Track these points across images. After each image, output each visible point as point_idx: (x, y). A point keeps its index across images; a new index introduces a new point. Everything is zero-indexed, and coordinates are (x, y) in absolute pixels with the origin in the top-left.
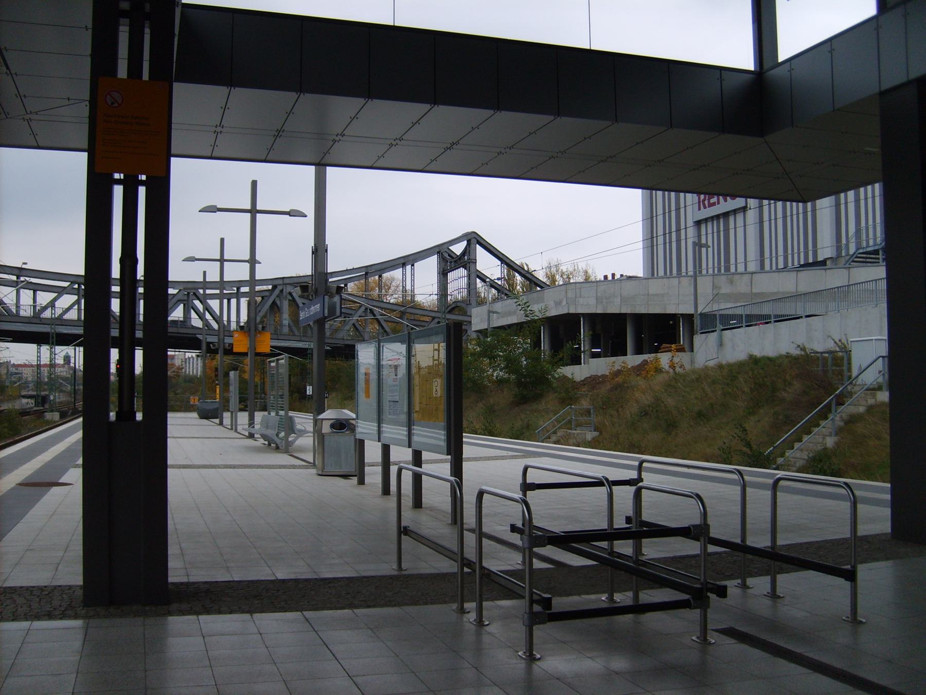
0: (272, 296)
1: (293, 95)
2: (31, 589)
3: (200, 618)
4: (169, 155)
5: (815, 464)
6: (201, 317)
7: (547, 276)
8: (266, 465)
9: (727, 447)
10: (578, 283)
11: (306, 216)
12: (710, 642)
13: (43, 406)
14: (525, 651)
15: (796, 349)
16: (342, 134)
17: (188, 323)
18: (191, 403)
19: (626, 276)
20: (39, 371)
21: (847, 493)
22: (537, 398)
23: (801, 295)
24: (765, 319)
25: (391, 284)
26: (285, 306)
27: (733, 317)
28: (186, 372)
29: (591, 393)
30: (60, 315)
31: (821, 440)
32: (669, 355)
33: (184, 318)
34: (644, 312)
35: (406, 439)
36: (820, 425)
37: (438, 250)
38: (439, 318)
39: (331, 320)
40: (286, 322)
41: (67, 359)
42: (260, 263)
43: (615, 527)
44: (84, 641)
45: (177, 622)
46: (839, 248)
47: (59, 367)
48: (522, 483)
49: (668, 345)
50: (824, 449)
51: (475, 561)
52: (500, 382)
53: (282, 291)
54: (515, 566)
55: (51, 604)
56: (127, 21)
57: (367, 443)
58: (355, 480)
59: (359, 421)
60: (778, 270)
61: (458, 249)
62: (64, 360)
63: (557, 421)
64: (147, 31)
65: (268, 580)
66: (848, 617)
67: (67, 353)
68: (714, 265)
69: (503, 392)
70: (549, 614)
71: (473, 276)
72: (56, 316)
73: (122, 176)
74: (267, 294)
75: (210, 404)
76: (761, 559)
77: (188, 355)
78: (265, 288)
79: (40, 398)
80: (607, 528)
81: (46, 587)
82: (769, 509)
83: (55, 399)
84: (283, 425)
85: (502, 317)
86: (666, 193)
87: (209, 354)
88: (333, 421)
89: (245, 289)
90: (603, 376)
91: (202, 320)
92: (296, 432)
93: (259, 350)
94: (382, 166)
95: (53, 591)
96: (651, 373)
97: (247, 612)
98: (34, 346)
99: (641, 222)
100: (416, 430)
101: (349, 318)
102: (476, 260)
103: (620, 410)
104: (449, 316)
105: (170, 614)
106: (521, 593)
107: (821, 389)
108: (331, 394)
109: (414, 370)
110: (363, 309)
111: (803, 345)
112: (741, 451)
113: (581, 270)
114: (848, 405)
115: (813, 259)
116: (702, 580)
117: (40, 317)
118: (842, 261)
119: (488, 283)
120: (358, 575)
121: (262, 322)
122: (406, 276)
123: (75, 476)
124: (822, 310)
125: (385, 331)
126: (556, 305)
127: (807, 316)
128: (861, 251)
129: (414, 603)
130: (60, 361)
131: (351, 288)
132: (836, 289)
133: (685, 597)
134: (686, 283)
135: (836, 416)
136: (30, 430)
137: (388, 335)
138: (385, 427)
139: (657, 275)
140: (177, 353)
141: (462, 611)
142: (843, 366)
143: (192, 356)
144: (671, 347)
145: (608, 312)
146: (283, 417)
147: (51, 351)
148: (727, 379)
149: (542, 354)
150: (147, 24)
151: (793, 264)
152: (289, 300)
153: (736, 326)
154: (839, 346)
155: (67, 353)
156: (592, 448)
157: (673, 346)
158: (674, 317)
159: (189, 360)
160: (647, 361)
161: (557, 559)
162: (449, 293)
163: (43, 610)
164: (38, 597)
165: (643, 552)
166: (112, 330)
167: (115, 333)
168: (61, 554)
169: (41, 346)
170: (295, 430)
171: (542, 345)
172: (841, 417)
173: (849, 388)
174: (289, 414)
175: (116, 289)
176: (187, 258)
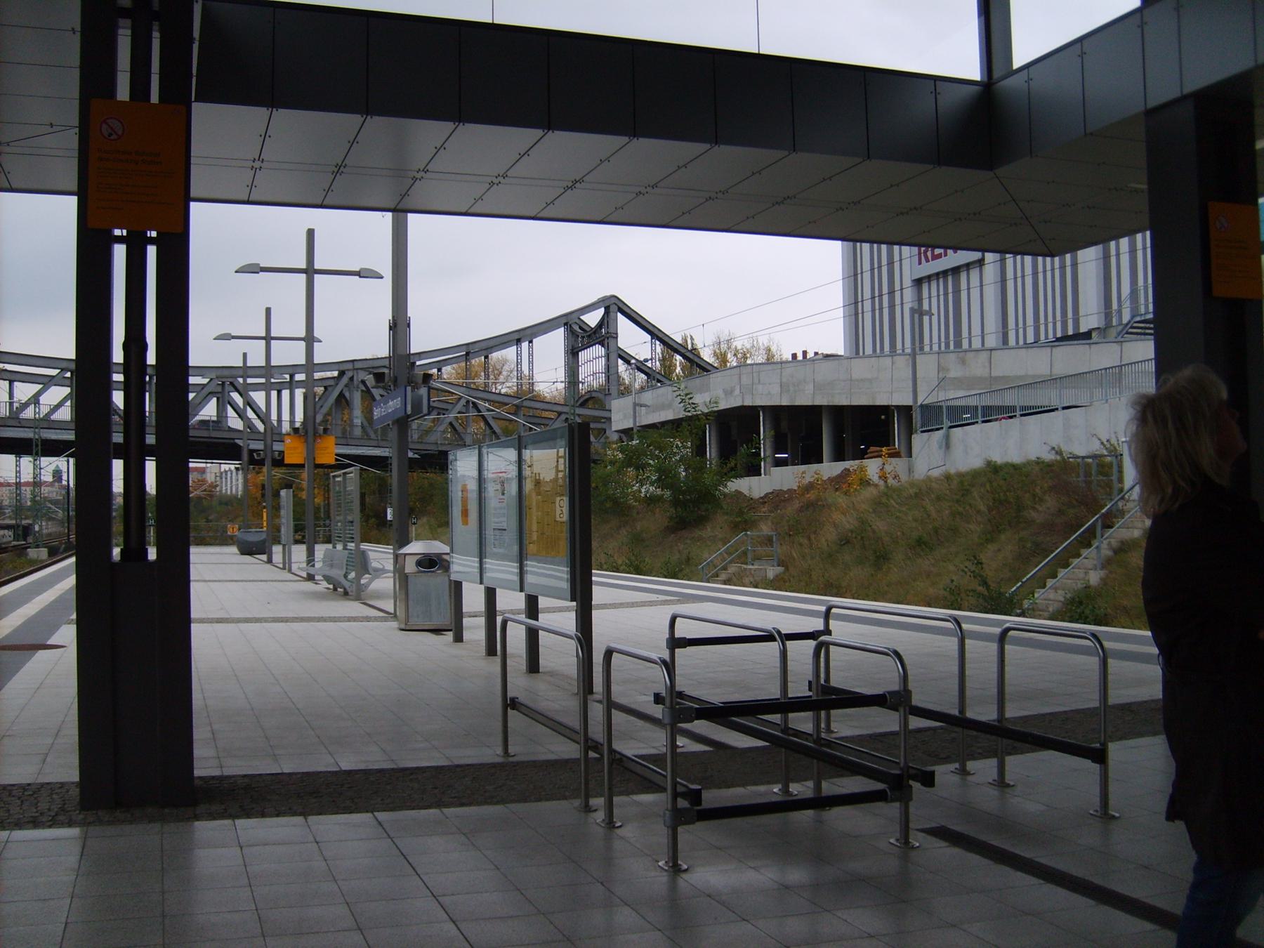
0: (339, 386)
1: (357, 119)
2: (9, 788)
3: (236, 824)
4: (187, 199)
5: (1074, 608)
6: (241, 414)
7: (715, 354)
8: (330, 617)
9: (956, 586)
10: (757, 364)
11: (382, 278)
12: (913, 846)
13: (25, 540)
14: (667, 860)
15: (1049, 453)
16: (425, 170)
17: (224, 423)
18: (229, 533)
19: (822, 354)
20: (18, 492)
21: (1092, 644)
22: (701, 521)
23: (1056, 379)
24: (1008, 412)
25: (502, 368)
26: (357, 399)
27: (966, 409)
28: (221, 491)
29: (772, 514)
30: (46, 414)
31: (1082, 575)
32: (878, 461)
33: (218, 416)
34: (845, 403)
35: (516, 578)
36: (1081, 556)
37: (565, 322)
38: (567, 413)
39: (419, 418)
40: (358, 421)
41: (57, 474)
42: (321, 341)
43: (790, 696)
44: (82, 855)
45: (206, 829)
46: (1108, 316)
47: (46, 486)
48: (669, 638)
49: (878, 449)
50: (1086, 587)
51: (602, 742)
52: (651, 500)
53: (352, 379)
54: (661, 748)
55: (36, 808)
56: (128, 22)
57: (465, 585)
58: (449, 636)
59: (454, 555)
60: (1027, 346)
61: (592, 319)
62: (54, 477)
63: (727, 553)
64: (156, 35)
65: (330, 772)
66: (1097, 811)
67: (57, 466)
68: (1017, 324)
69: (655, 514)
70: (699, 811)
71: (613, 356)
72: (41, 416)
73: (125, 233)
74: (332, 382)
75: (254, 537)
76: (988, 736)
77: (224, 467)
78: (329, 374)
79: (21, 528)
80: (779, 697)
81: (29, 785)
82: (957, 662)
83: (41, 529)
84: (353, 562)
85: (654, 412)
86: (875, 245)
87: (252, 466)
88: (420, 556)
89: (300, 377)
90: (790, 491)
91: (242, 420)
92: (371, 571)
93: (319, 461)
94: (479, 211)
95: (39, 790)
96: (855, 487)
97: (300, 814)
98: (12, 458)
99: (841, 281)
100: (530, 565)
101: (444, 414)
102: (617, 334)
103: (813, 536)
104: (579, 411)
105: (197, 818)
106: (662, 784)
107: (1082, 507)
108: (420, 519)
109: (528, 486)
110: (463, 402)
111: (1059, 447)
112: (974, 591)
113: (762, 347)
114: (1118, 528)
115: (1073, 330)
116: (902, 765)
117: (18, 418)
118: (1113, 333)
119: (633, 366)
120: (450, 763)
121: (325, 421)
122: (521, 357)
123: (67, 635)
124: (1081, 400)
125: (494, 432)
126: (726, 395)
127: (1064, 408)
128: (1138, 319)
129: (524, 799)
130: (47, 477)
131: (448, 374)
132: (1103, 371)
133: (880, 786)
134: (902, 363)
135: (1102, 542)
136: (8, 573)
137: (498, 438)
138: (489, 563)
139: (864, 353)
140: (209, 465)
141: (588, 809)
142: (1112, 475)
143: (230, 468)
144: (882, 451)
145: (797, 404)
146: (353, 552)
147: (34, 464)
148: (956, 494)
149: (708, 463)
150: (156, 26)
151: (1047, 338)
152: (362, 391)
153: (968, 422)
154: (1107, 449)
155: (57, 466)
156: (775, 590)
157: (883, 449)
158: (886, 409)
159: (226, 475)
160: (849, 470)
161: (718, 739)
162: (580, 380)
163: (26, 815)
164: (19, 798)
165: (832, 729)
166: (114, 434)
167: (118, 438)
168: (50, 741)
169: (20, 457)
170: (369, 569)
171: (708, 449)
172: (1109, 544)
173: (1120, 504)
174: (362, 547)
175: (118, 377)
176: (221, 335)
